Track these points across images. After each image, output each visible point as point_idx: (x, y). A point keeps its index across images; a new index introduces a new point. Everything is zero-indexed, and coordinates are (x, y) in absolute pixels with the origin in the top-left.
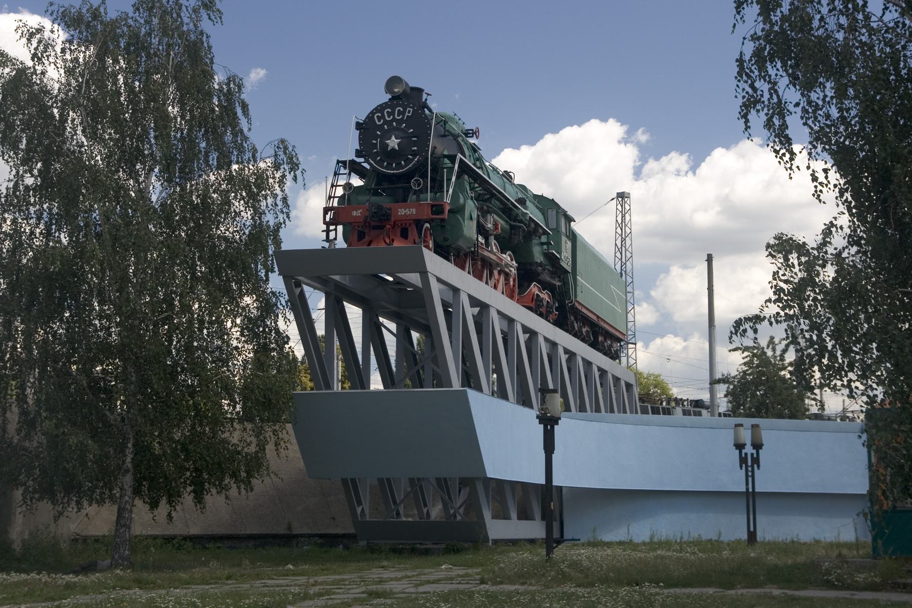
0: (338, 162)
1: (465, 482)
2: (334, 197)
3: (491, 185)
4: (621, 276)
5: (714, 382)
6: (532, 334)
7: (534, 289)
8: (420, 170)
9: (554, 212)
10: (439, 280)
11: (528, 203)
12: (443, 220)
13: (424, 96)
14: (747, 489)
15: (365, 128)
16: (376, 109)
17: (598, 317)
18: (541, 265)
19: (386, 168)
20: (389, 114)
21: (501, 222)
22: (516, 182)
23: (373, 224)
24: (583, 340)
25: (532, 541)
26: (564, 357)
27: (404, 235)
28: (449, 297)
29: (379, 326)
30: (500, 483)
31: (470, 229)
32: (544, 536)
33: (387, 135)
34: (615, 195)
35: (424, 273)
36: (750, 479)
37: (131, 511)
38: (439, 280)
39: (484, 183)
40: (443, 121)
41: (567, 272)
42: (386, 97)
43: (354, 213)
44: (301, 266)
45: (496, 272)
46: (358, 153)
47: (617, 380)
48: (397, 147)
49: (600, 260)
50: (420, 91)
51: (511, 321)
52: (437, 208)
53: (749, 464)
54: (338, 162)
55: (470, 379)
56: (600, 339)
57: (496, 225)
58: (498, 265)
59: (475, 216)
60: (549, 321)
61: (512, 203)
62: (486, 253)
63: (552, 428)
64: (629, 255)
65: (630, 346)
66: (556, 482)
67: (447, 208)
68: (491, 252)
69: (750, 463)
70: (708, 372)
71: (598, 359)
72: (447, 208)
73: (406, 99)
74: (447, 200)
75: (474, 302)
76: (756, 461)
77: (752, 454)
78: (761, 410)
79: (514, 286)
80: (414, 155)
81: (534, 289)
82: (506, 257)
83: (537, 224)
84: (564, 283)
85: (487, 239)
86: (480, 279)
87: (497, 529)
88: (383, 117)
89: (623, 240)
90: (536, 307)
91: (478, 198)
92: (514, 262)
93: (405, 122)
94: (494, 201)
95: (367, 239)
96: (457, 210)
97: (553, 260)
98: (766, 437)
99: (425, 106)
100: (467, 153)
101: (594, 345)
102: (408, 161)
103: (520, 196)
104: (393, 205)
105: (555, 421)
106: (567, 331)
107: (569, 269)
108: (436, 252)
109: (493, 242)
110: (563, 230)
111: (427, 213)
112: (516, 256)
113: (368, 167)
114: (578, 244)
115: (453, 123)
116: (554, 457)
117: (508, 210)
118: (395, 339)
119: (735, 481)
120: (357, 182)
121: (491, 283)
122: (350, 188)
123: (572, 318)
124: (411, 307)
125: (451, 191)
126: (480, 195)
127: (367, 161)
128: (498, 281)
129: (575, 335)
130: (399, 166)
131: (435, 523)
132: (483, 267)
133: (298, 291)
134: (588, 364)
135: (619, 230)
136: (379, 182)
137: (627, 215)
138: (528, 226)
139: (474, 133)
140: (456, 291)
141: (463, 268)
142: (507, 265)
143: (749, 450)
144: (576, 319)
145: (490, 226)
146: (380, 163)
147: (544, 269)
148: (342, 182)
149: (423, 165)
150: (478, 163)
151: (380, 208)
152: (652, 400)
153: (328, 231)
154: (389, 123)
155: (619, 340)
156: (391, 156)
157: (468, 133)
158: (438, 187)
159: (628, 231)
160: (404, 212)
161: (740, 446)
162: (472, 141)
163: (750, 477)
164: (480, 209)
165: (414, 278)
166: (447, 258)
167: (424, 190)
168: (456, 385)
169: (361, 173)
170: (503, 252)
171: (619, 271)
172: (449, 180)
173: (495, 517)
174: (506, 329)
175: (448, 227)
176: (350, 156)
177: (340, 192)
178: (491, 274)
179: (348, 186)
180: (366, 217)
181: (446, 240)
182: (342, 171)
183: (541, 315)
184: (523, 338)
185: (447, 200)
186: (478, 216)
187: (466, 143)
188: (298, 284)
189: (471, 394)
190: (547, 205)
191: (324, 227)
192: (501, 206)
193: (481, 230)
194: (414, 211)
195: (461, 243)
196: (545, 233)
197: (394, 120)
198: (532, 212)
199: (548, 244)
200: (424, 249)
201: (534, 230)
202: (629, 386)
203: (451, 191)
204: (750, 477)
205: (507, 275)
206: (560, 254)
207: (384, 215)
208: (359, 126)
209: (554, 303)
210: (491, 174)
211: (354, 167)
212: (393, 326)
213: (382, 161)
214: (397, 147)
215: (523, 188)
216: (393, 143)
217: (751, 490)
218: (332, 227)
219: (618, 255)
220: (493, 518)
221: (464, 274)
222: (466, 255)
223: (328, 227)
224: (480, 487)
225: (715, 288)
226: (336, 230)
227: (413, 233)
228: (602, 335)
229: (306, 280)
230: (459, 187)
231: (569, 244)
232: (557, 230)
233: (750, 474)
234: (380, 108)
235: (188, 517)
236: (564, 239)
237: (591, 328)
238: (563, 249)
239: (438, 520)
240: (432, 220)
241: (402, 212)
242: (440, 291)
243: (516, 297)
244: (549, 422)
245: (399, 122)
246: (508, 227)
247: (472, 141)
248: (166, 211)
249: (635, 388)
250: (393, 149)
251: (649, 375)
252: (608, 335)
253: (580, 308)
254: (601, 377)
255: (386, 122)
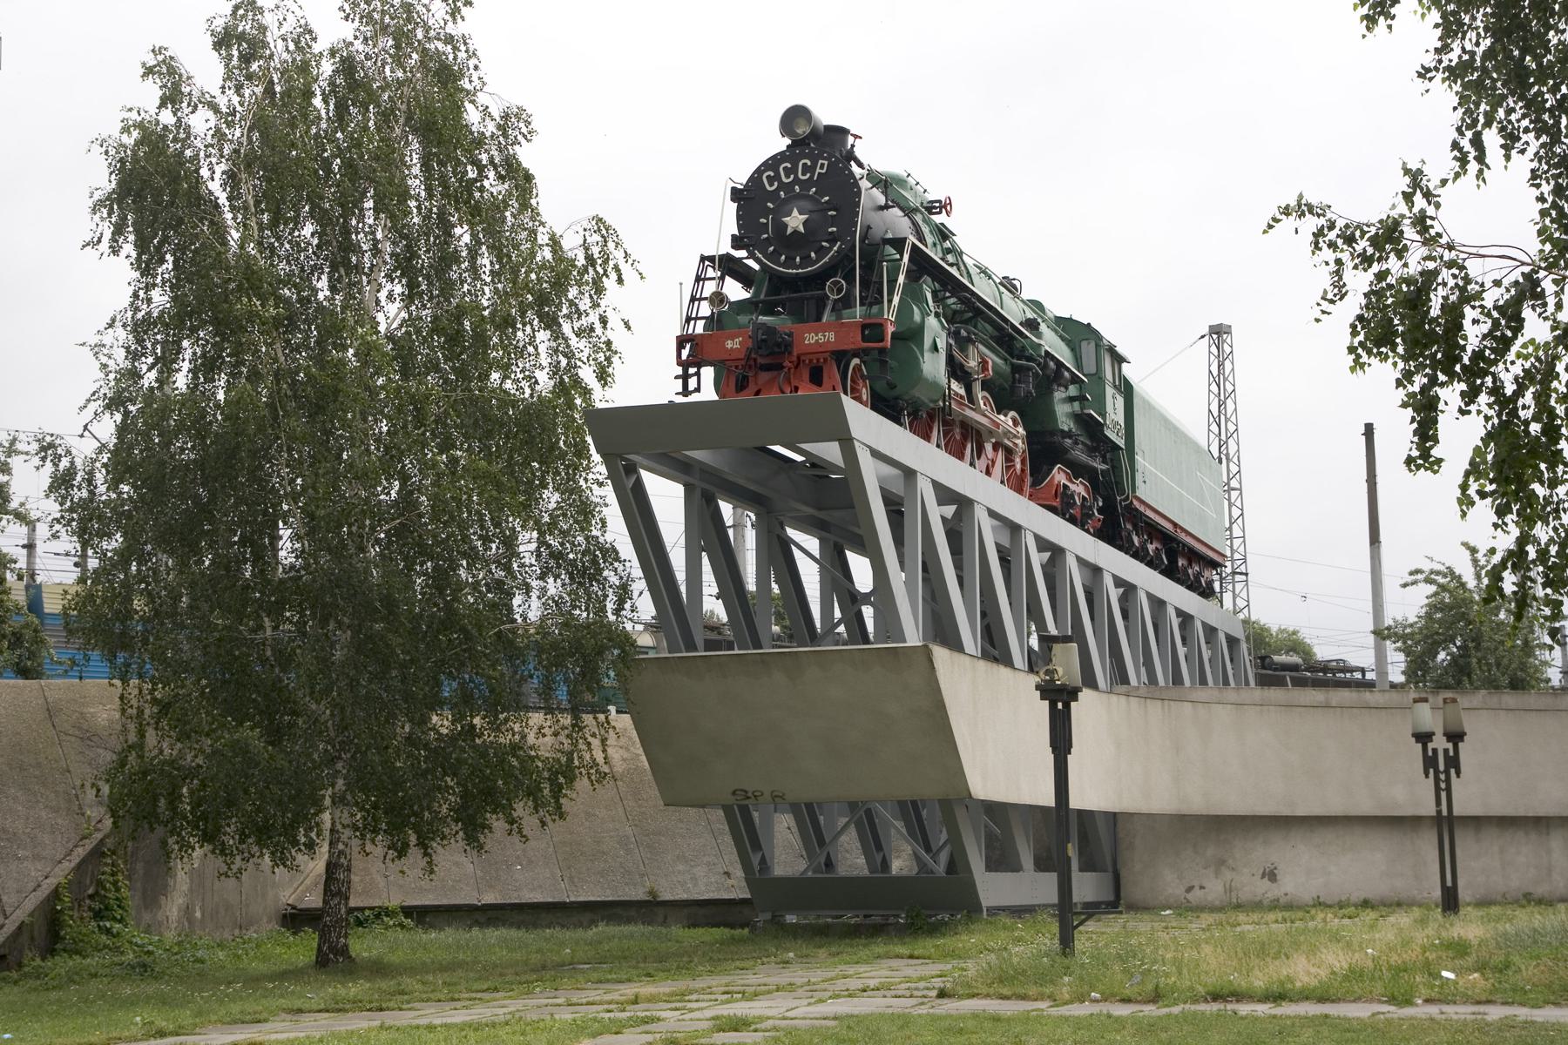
0: (703, 258)
1: (947, 805)
2: (697, 318)
3: (973, 294)
4: (1220, 461)
5: (1381, 634)
6: (1056, 553)
7: (1059, 476)
8: (842, 264)
9: (1093, 344)
10: (876, 454)
11: (1043, 327)
12: (882, 351)
13: (851, 140)
14: (1439, 812)
15: (748, 198)
16: (765, 164)
17: (1175, 525)
18: (1068, 434)
19: (784, 265)
20: (788, 172)
21: (992, 359)
22: (1025, 296)
23: (761, 361)
24: (1150, 564)
25: (1029, 910)
26: (1114, 594)
27: (817, 378)
28: (898, 488)
29: (786, 545)
30: (995, 810)
31: (934, 366)
32: (1055, 900)
33: (783, 208)
34: (1206, 330)
35: (847, 443)
36: (1444, 794)
37: (349, 869)
38: (876, 454)
39: (957, 288)
40: (884, 183)
41: (1116, 447)
42: (783, 143)
43: (729, 344)
44: (637, 438)
45: (988, 447)
46: (737, 242)
47: (1210, 631)
48: (802, 229)
49: (1176, 428)
50: (843, 132)
51: (1015, 529)
52: (873, 330)
53: (1442, 767)
54: (703, 258)
55: (942, 630)
56: (1181, 562)
57: (983, 364)
58: (991, 432)
59: (941, 344)
60: (1087, 531)
61: (1013, 326)
62: (969, 413)
63: (1067, 706)
64: (1232, 428)
65: (1238, 578)
66: (1075, 802)
67: (890, 329)
68: (977, 410)
69: (1442, 766)
70: (1371, 616)
71: (1177, 596)
72: (890, 329)
73: (815, 148)
74: (890, 315)
75: (945, 494)
76: (1453, 762)
77: (1446, 751)
78: (1460, 675)
79: (1023, 470)
80: (833, 241)
81: (1059, 476)
82: (1006, 420)
83: (1060, 364)
84: (1113, 467)
85: (969, 389)
86: (961, 457)
87: (993, 888)
88: (777, 177)
89: (1222, 404)
90: (1062, 506)
91: (951, 318)
92: (1020, 429)
93: (815, 184)
94: (981, 323)
95: (752, 388)
96: (911, 336)
97: (1092, 428)
98: (1469, 724)
99: (851, 156)
100: (930, 239)
101: (1170, 572)
102: (821, 252)
103: (1030, 315)
104: (796, 328)
105: (1072, 694)
106: (1120, 548)
107: (1121, 443)
108: (874, 408)
109: (980, 395)
110: (1109, 375)
111: (855, 341)
112: (1026, 418)
113: (756, 267)
114: (1135, 401)
115: (904, 188)
116: (1072, 760)
117: (1006, 338)
118: (816, 567)
119: (1418, 797)
120: (735, 291)
121: (982, 463)
122: (722, 301)
123: (1129, 526)
124: (833, 505)
125: (896, 300)
126: (955, 312)
127: (751, 256)
128: (993, 462)
129: (1135, 556)
130: (806, 260)
131: (900, 880)
132: (965, 437)
133: (631, 482)
134: (1158, 604)
135: (1214, 388)
136: (776, 291)
137: (1227, 363)
138: (1044, 367)
139: (944, 206)
140: (909, 474)
141: (927, 438)
142: (1007, 433)
143: (1440, 743)
144: (1135, 526)
145: (972, 364)
146: (773, 257)
147: (1076, 443)
148: (709, 288)
149: (845, 260)
150: (950, 258)
151: (770, 331)
152: (1282, 667)
153: (685, 377)
154: (788, 187)
155: (1214, 565)
156: (791, 243)
157: (932, 208)
158: (873, 295)
159: (1229, 388)
160: (815, 338)
161: (1423, 738)
162: (937, 219)
163: (1443, 789)
164: (955, 335)
165: (830, 451)
166: (897, 420)
167: (847, 302)
168: (913, 637)
169: (744, 277)
170: (1000, 409)
171: (1216, 455)
172: (892, 282)
173: (989, 868)
174: (1006, 543)
175: (892, 363)
176: (726, 248)
177: (705, 309)
178: (980, 450)
179: (718, 298)
180: (749, 351)
181: (892, 386)
182: (710, 273)
183: (1072, 520)
184: (1038, 559)
185: (890, 315)
186: (949, 346)
187: (928, 222)
188: (631, 469)
189: (940, 654)
190: (1077, 332)
191: (679, 371)
192: (996, 333)
193: (956, 369)
194: (831, 336)
195: (920, 394)
196: (1075, 380)
197: (797, 181)
198: (1050, 342)
199: (1081, 398)
200: (847, 401)
201: (1054, 375)
202: (1232, 641)
203: (896, 300)
204: (1443, 789)
205: (1009, 452)
206: (1103, 415)
207: (779, 345)
208: (736, 195)
209: (1095, 499)
210: (975, 279)
211: (728, 266)
212: (812, 544)
213: (777, 253)
214: (802, 229)
215: (1037, 305)
216: (795, 221)
217: (1445, 813)
218: (692, 370)
219: (1214, 428)
220: (989, 868)
221: (963, 466)
222: (931, 417)
223: (685, 371)
224: (961, 815)
225: (1378, 479)
226: (698, 374)
227: (832, 373)
228: (1184, 556)
229: (645, 462)
230: (913, 293)
231: (1120, 401)
232: (1098, 377)
233: (1443, 786)
234: (773, 163)
235: (455, 874)
236: (1110, 391)
237: (1164, 545)
238: (1109, 408)
239: (905, 873)
240: (866, 351)
241: (811, 338)
242: (994, 528)
243: (1027, 489)
244: (1059, 697)
245: (805, 185)
246: (1006, 368)
247: (937, 219)
248: (403, 348)
249: (1244, 646)
250: (795, 232)
251: (1281, 631)
252: (1194, 556)
253: (1142, 509)
254: (1182, 626)
255: (782, 186)
